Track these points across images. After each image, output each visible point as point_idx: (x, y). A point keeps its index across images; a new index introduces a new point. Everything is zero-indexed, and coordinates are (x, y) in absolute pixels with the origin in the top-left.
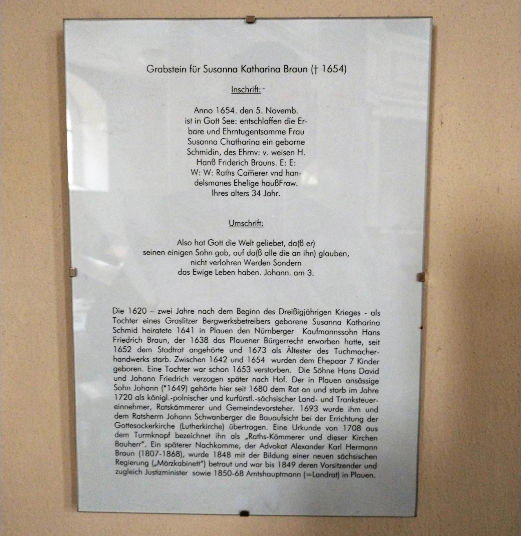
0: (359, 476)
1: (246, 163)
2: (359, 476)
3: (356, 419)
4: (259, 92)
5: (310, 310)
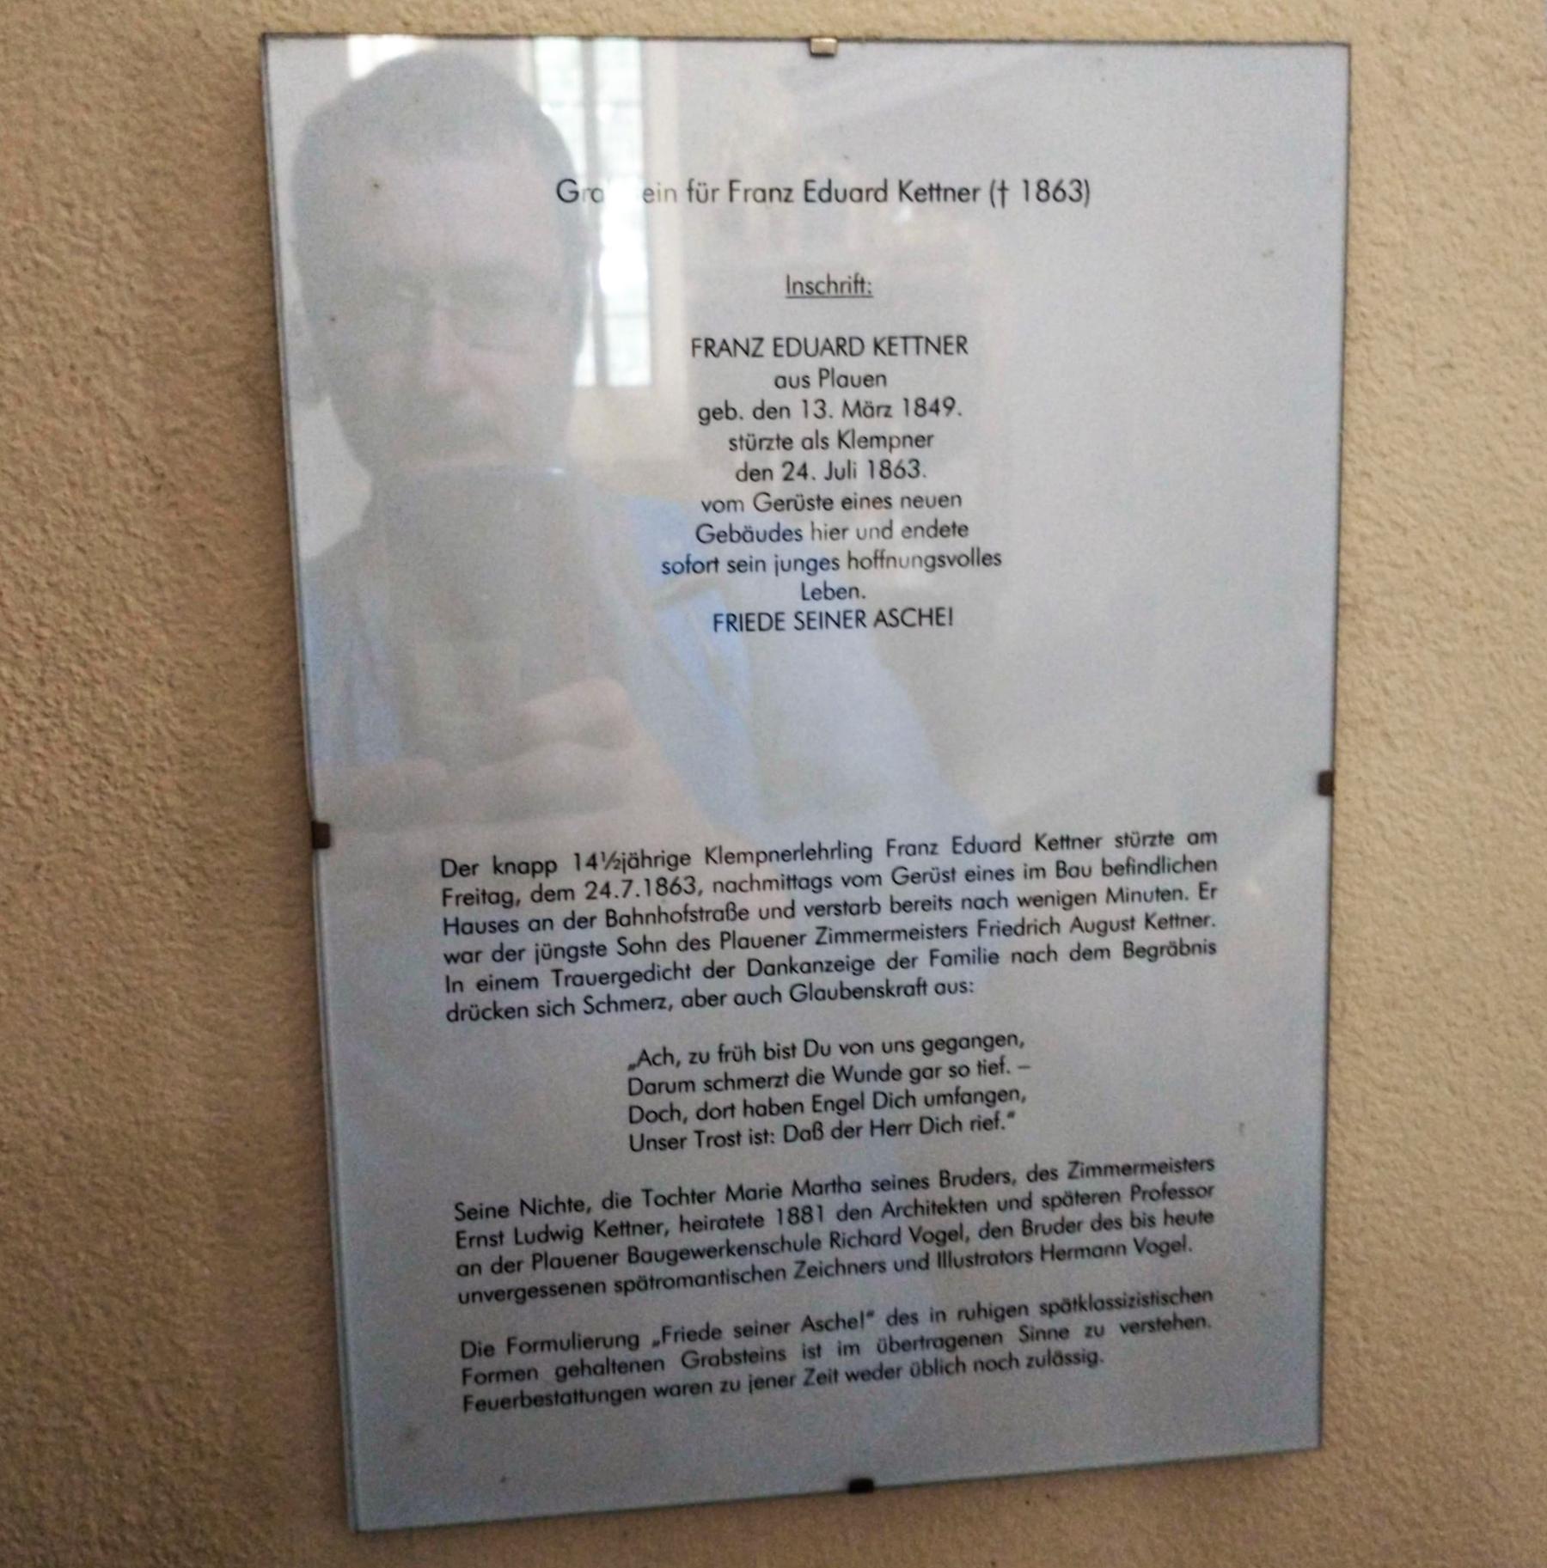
0: (556, 1263)
1: (569, 1009)
2: (556, 1263)
3: (773, 910)
4: (866, 293)
5: (639, 856)
